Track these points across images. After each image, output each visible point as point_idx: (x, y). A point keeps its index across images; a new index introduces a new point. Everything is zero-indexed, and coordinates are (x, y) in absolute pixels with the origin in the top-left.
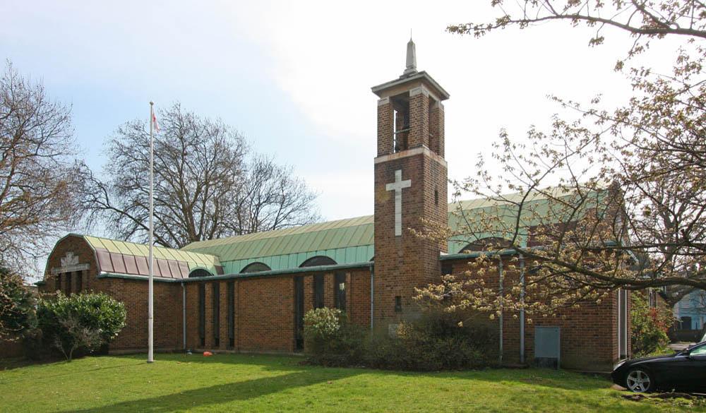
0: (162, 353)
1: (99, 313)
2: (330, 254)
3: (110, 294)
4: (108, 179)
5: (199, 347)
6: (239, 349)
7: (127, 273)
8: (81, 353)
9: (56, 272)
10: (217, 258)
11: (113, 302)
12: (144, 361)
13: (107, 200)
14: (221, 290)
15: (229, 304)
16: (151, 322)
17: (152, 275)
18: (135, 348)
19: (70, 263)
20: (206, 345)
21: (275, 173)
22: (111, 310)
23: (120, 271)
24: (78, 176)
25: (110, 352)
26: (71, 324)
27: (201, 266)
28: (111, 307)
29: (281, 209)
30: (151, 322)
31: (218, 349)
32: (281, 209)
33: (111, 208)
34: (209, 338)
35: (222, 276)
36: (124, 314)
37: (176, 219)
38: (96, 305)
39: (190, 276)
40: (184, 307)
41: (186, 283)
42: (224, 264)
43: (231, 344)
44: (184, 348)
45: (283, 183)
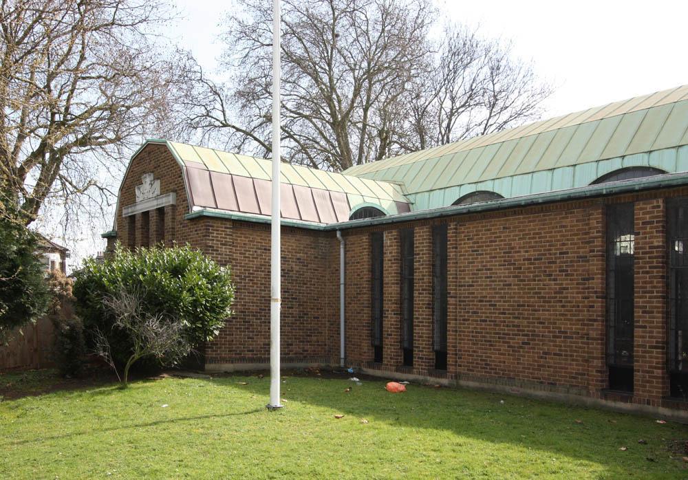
0: (308, 374)
1: (182, 288)
2: (655, 162)
3: (207, 250)
4: (227, 80)
5: (370, 365)
6: (457, 376)
7: (240, 211)
8: (148, 369)
9: (128, 212)
10: (398, 188)
11: (211, 265)
12: (257, 400)
13: (223, 111)
14: (416, 243)
15: (433, 274)
16: (276, 309)
17: (279, 212)
18: (252, 360)
19: (149, 196)
20: (385, 362)
21: (480, 51)
22: (204, 281)
23: (227, 207)
24: (184, 76)
25: (208, 366)
26: (124, 307)
27: (372, 202)
28: (206, 276)
29: (490, 117)
30: (276, 309)
31: (410, 372)
32: (490, 117)
33: (229, 126)
34: (391, 349)
35: (407, 214)
36: (229, 290)
37: (321, 143)
38: (177, 271)
39: (351, 218)
40: (342, 281)
41: (346, 231)
42: (412, 199)
43: (440, 363)
44: (342, 364)
45: (495, 70)
